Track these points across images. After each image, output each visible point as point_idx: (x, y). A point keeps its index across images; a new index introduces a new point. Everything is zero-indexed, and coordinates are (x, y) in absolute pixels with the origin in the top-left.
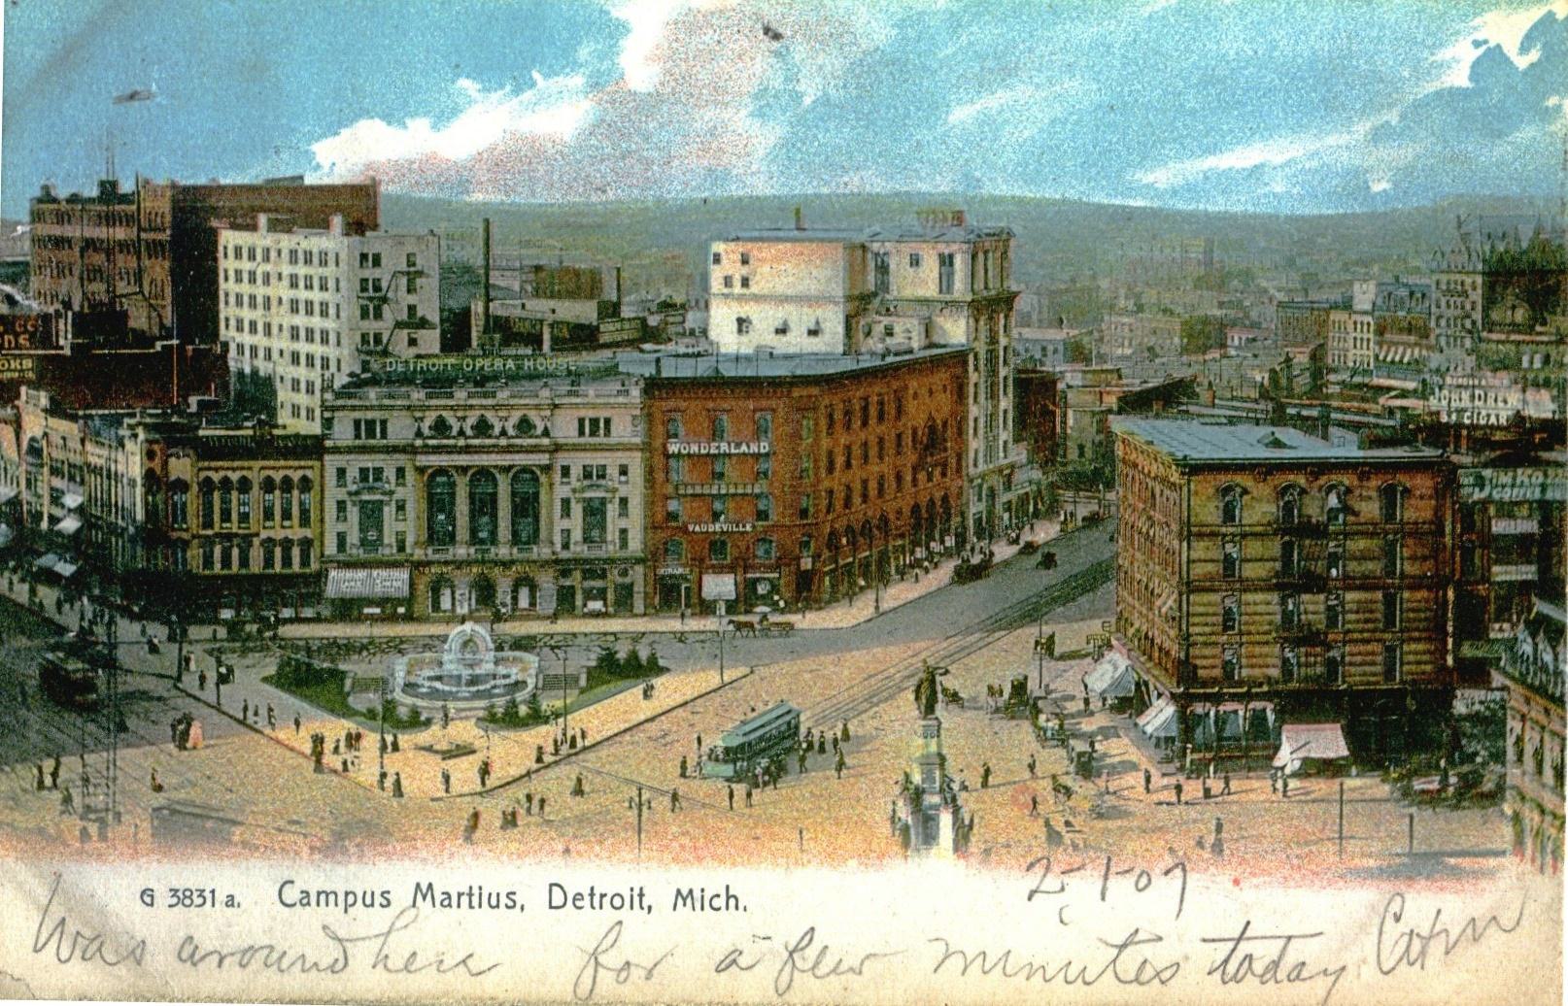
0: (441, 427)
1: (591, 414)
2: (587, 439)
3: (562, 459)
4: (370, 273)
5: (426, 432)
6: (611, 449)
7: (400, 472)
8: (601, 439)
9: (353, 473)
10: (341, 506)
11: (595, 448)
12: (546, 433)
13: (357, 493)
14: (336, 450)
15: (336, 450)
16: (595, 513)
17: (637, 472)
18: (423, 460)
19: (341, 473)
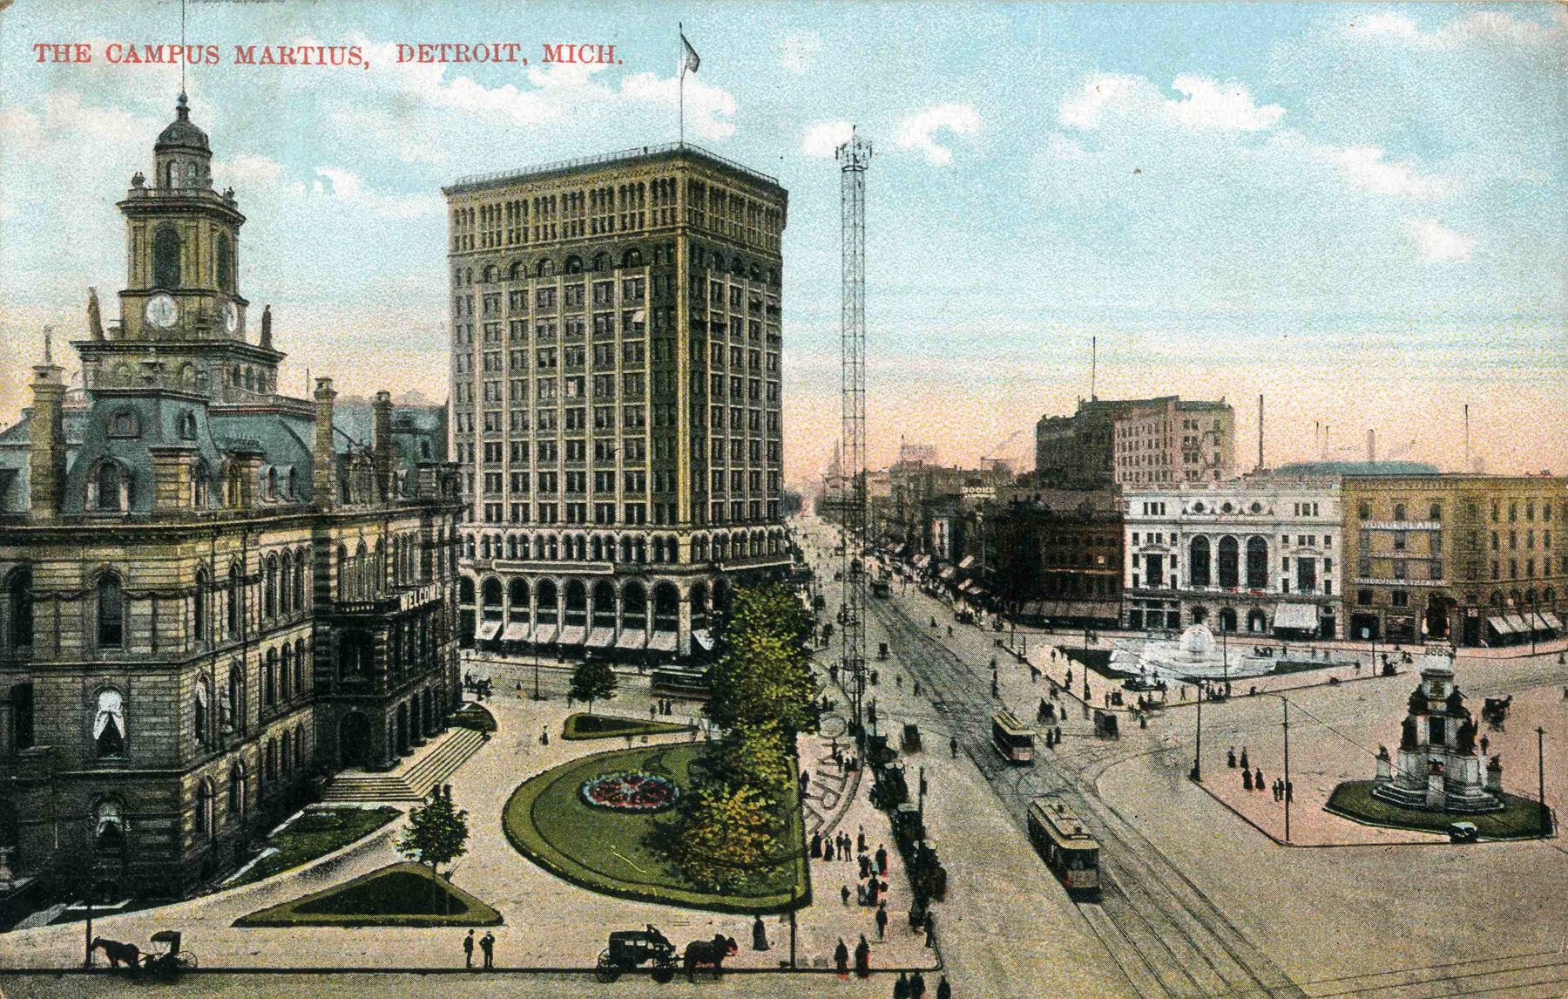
0: (1199, 508)
1: (1153, 500)
2: (1150, 517)
3: (1283, 530)
4: (1191, 432)
5: (1189, 510)
6: (1317, 525)
7: (1174, 537)
8: (1311, 518)
9: (1143, 537)
10: (1136, 557)
11: (1154, 522)
12: (1271, 512)
13: (1297, 552)
14: (1132, 522)
15: (1132, 522)
16: (1154, 564)
17: (1336, 541)
18: (1186, 529)
19: (1136, 536)
